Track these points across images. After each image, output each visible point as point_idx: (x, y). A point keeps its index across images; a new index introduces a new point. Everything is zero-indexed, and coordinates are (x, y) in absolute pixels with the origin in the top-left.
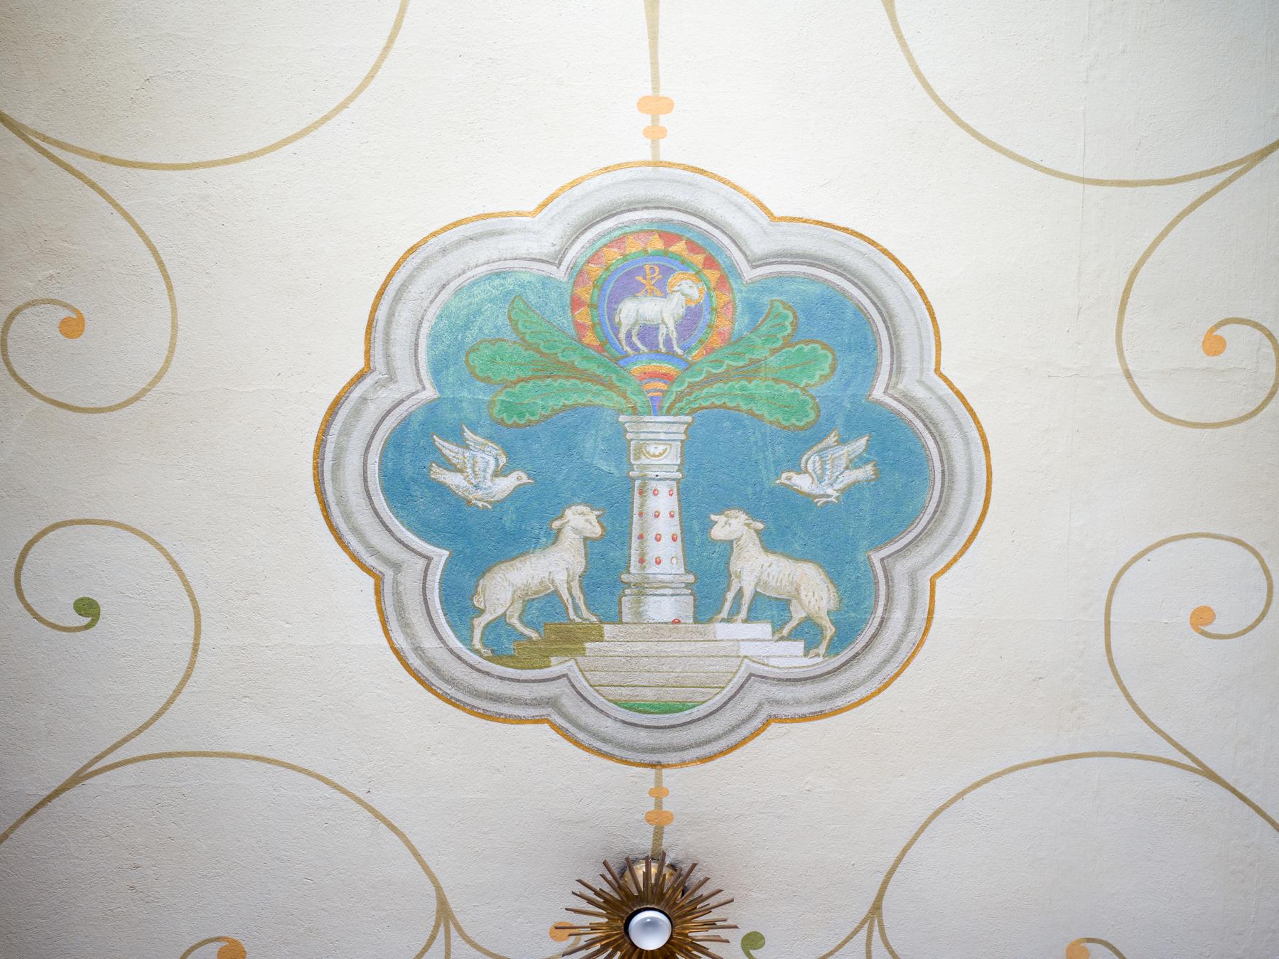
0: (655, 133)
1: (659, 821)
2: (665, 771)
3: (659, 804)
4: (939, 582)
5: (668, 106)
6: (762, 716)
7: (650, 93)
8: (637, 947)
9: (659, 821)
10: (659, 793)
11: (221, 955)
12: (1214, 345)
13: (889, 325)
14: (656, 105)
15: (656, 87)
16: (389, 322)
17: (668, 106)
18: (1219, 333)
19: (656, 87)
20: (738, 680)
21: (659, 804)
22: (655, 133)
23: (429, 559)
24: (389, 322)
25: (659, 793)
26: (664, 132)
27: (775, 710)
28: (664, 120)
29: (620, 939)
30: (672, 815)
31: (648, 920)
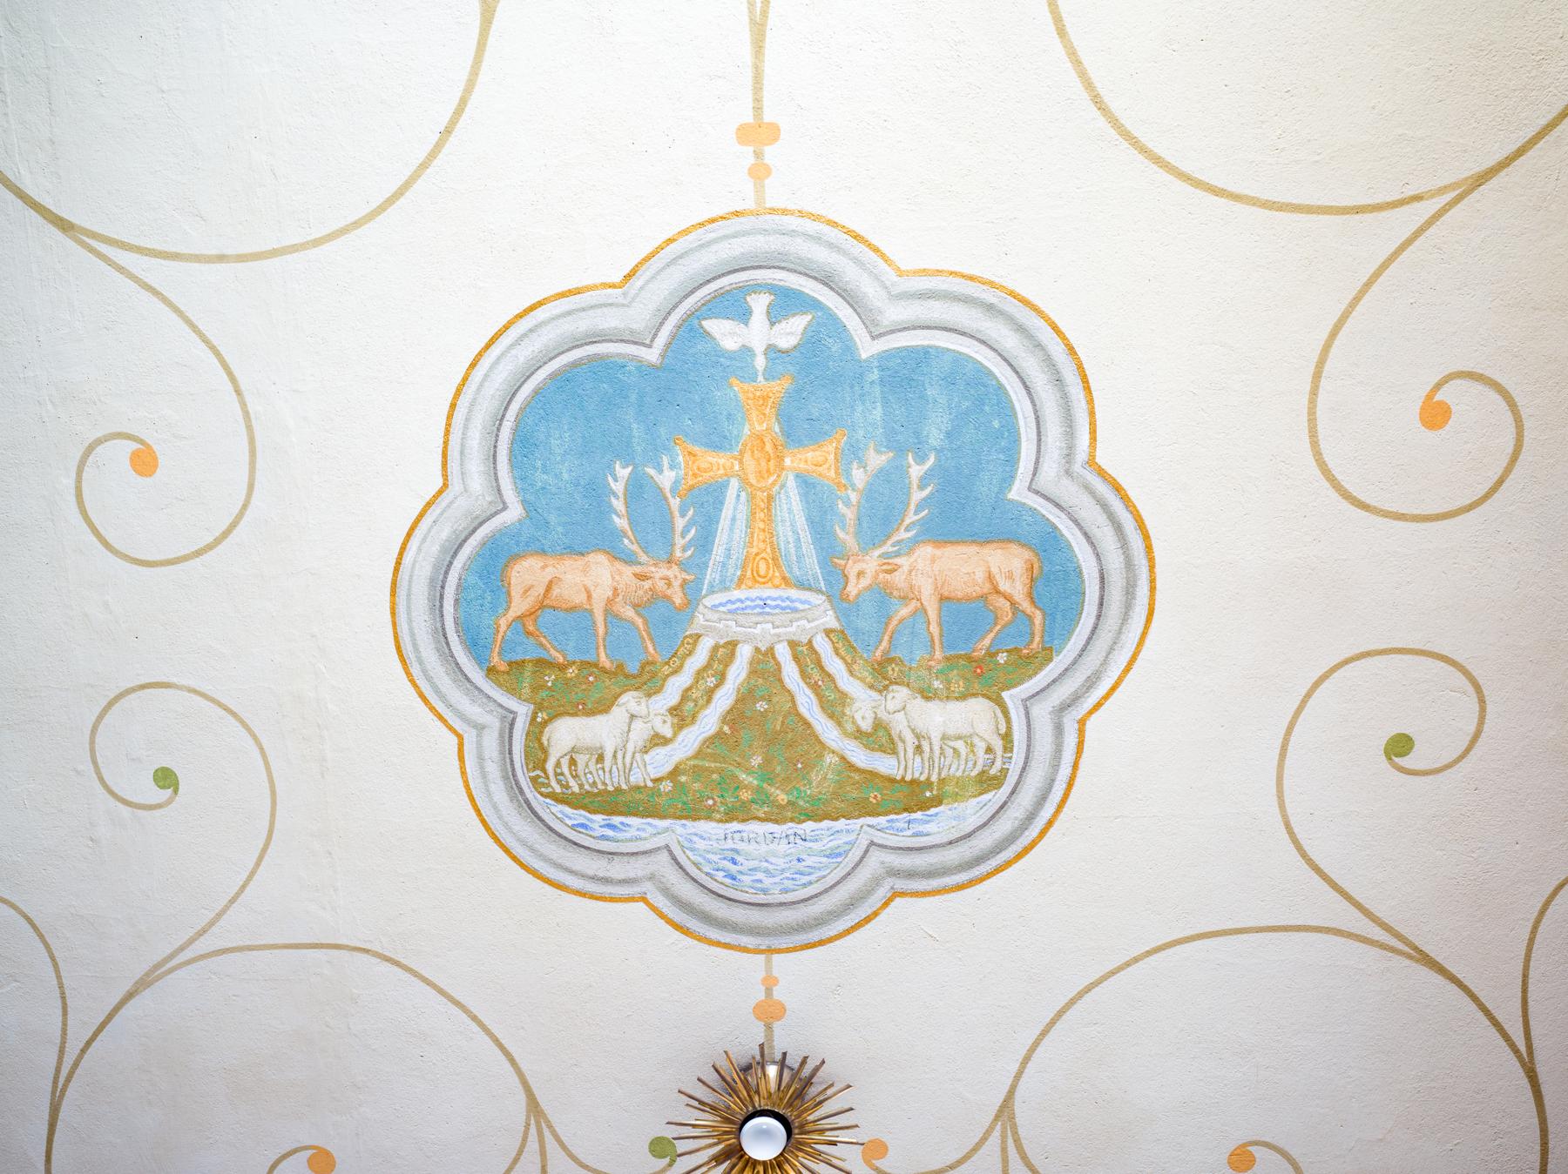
0: (759, 172)
1: (769, 1012)
2: (776, 957)
3: (769, 992)
4: (1089, 725)
5: (773, 133)
6: (882, 893)
7: (750, 119)
8: (742, 1150)
9: (769, 1012)
10: (770, 983)
11: (311, 1162)
12: (1435, 415)
13: (507, 755)
14: (759, 133)
15: (758, 109)
16: (583, 876)
17: (773, 133)
18: (1438, 397)
19: (758, 109)
20: (856, 854)
21: (769, 992)
22: (759, 172)
23: (872, 843)
24: (583, 876)
25: (770, 983)
26: (768, 171)
27: (900, 884)
28: (771, 153)
29: (735, 1153)
30: (783, 1009)
31: (765, 1127)
